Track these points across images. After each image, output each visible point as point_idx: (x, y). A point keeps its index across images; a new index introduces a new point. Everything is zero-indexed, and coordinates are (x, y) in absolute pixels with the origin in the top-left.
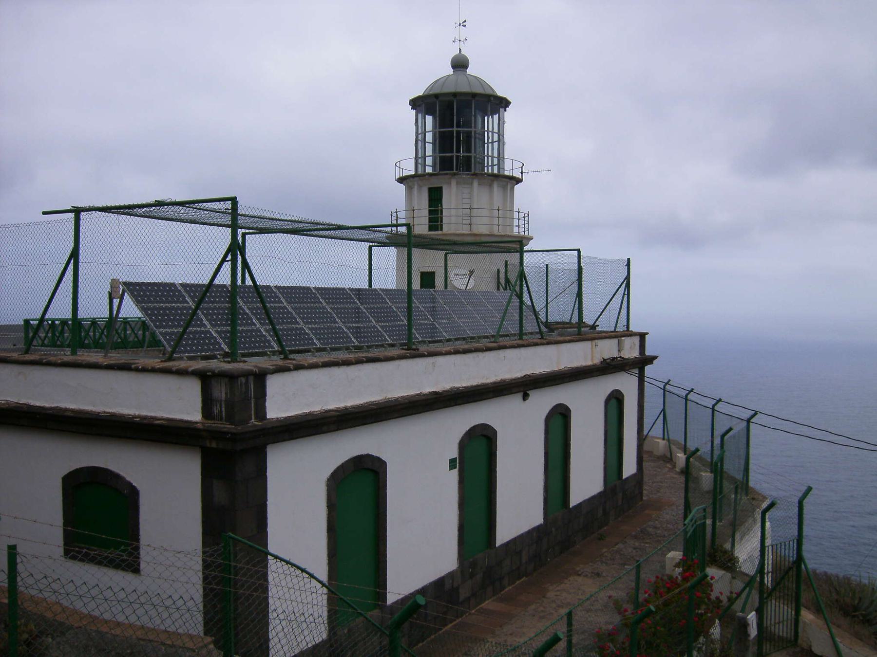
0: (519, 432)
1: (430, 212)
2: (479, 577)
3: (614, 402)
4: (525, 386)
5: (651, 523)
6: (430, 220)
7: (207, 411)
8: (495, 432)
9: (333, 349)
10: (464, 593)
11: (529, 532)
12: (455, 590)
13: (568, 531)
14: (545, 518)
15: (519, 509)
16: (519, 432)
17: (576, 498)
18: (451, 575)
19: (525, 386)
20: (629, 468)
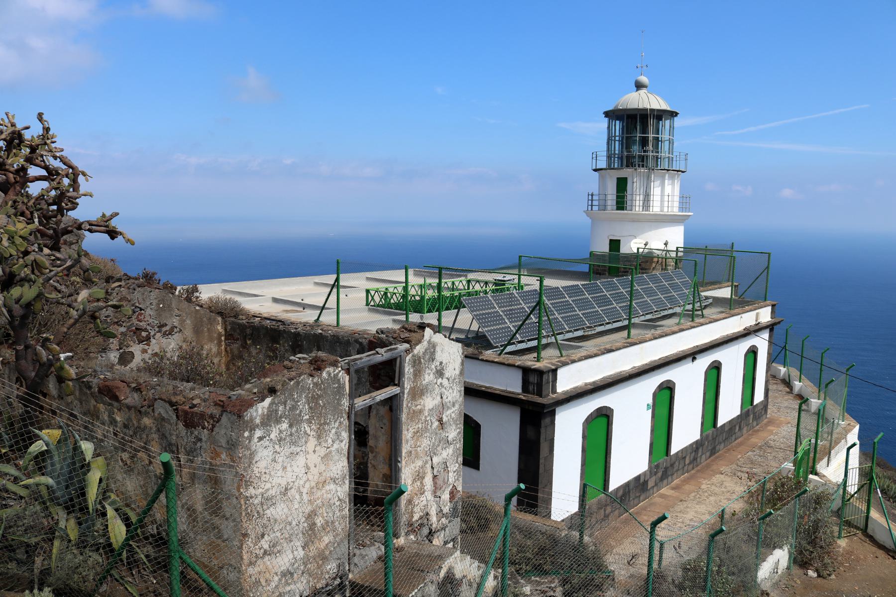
0: (689, 380)
1: (618, 197)
2: (660, 474)
3: (752, 355)
4: (693, 354)
5: (772, 437)
6: (617, 203)
7: (525, 389)
8: (674, 384)
9: (529, 340)
10: (651, 484)
11: (691, 445)
12: (646, 483)
13: (716, 439)
14: (701, 435)
15: (686, 431)
16: (689, 380)
17: (722, 420)
18: (645, 473)
19: (693, 354)
20: (759, 397)
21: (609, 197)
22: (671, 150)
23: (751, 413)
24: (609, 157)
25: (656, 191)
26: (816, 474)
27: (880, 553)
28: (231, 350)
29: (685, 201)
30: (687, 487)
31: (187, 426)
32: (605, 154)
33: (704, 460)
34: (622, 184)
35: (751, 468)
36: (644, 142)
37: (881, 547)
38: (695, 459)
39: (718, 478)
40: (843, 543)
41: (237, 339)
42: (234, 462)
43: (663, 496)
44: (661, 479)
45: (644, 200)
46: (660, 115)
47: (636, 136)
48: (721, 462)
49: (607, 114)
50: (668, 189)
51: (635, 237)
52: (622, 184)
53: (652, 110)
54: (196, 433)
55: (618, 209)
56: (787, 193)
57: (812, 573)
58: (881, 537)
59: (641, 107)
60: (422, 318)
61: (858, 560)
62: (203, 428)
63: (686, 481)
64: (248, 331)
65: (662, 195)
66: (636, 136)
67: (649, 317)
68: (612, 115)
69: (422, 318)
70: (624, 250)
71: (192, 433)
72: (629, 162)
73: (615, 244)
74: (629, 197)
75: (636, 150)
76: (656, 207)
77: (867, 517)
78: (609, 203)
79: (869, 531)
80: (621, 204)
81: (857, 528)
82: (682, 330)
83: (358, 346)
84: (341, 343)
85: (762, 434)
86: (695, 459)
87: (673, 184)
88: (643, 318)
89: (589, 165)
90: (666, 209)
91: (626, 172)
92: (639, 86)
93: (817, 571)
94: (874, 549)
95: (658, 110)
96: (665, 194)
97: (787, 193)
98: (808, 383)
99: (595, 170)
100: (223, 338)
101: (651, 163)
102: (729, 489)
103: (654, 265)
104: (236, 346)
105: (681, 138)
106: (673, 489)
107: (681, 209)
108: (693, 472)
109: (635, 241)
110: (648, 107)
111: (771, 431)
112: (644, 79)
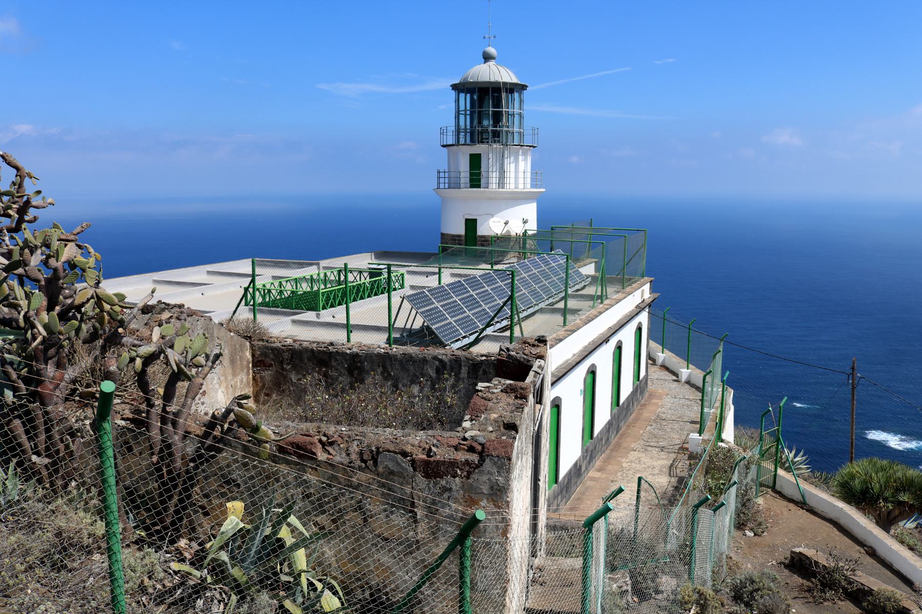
1: (479, 174)
6: (471, 180)
18: (580, 459)
20: (643, 373)
21: (462, 175)
22: (521, 125)
23: (640, 386)
24: (458, 131)
25: (510, 167)
26: (722, 441)
27: (791, 506)
28: (261, 378)
29: (537, 177)
30: (610, 467)
31: (427, 476)
32: (453, 129)
33: (614, 441)
34: (475, 161)
35: (658, 442)
36: (497, 117)
37: (791, 500)
38: (608, 439)
39: (633, 455)
40: (760, 501)
41: (271, 365)
42: (499, 507)
43: (592, 479)
44: (589, 463)
45: (500, 178)
46: (512, 89)
47: (486, 109)
48: (628, 439)
49: (454, 87)
50: (522, 164)
51: (492, 216)
52: (475, 161)
53: (505, 83)
54: (443, 483)
55: (472, 186)
56: (574, 159)
57: (750, 534)
58: (788, 491)
59: (492, 80)
60: (318, 316)
61: (776, 515)
62: (454, 477)
63: (608, 460)
64: (286, 355)
65: (517, 172)
66: (486, 109)
67: (551, 300)
68: (459, 88)
69: (318, 316)
70: (482, 231)
71: (436, 484)
72: (477, 136)
73: (471, 224)
74: (483, 174)
75: (488, 123)
76: (510, 186)
77: (775, 476)
78: (462, 181)
79: (778, 487)
80: (475, 181)
81: (768, 487)
82: (601, 313)
83: (437, 363)
84: (415, 362)
85: (650, 408)
86: (608, 439)
87: (525, 160)
88: (547, 302)
89: (437, 141)
90: (521, 186)
91: (478, 148)
92: (487, 58)
93: (752, 529)
94: (785, 503)
95: (511, 84)
96: (517, 171)
97: (574, 159)
98: (670, 354)
99: (444, 146)
100: (251, 365)
101: (503, 137)
102: (648, 464)
103: (512, 244)
104: (267, 374)
105: (529, 113)
106: (599, 470)
107: (532, 187)
108: (608, 452)
109: (492, 220)
110: (500, 80)
111: (657, 404)
112: (492, 50)
